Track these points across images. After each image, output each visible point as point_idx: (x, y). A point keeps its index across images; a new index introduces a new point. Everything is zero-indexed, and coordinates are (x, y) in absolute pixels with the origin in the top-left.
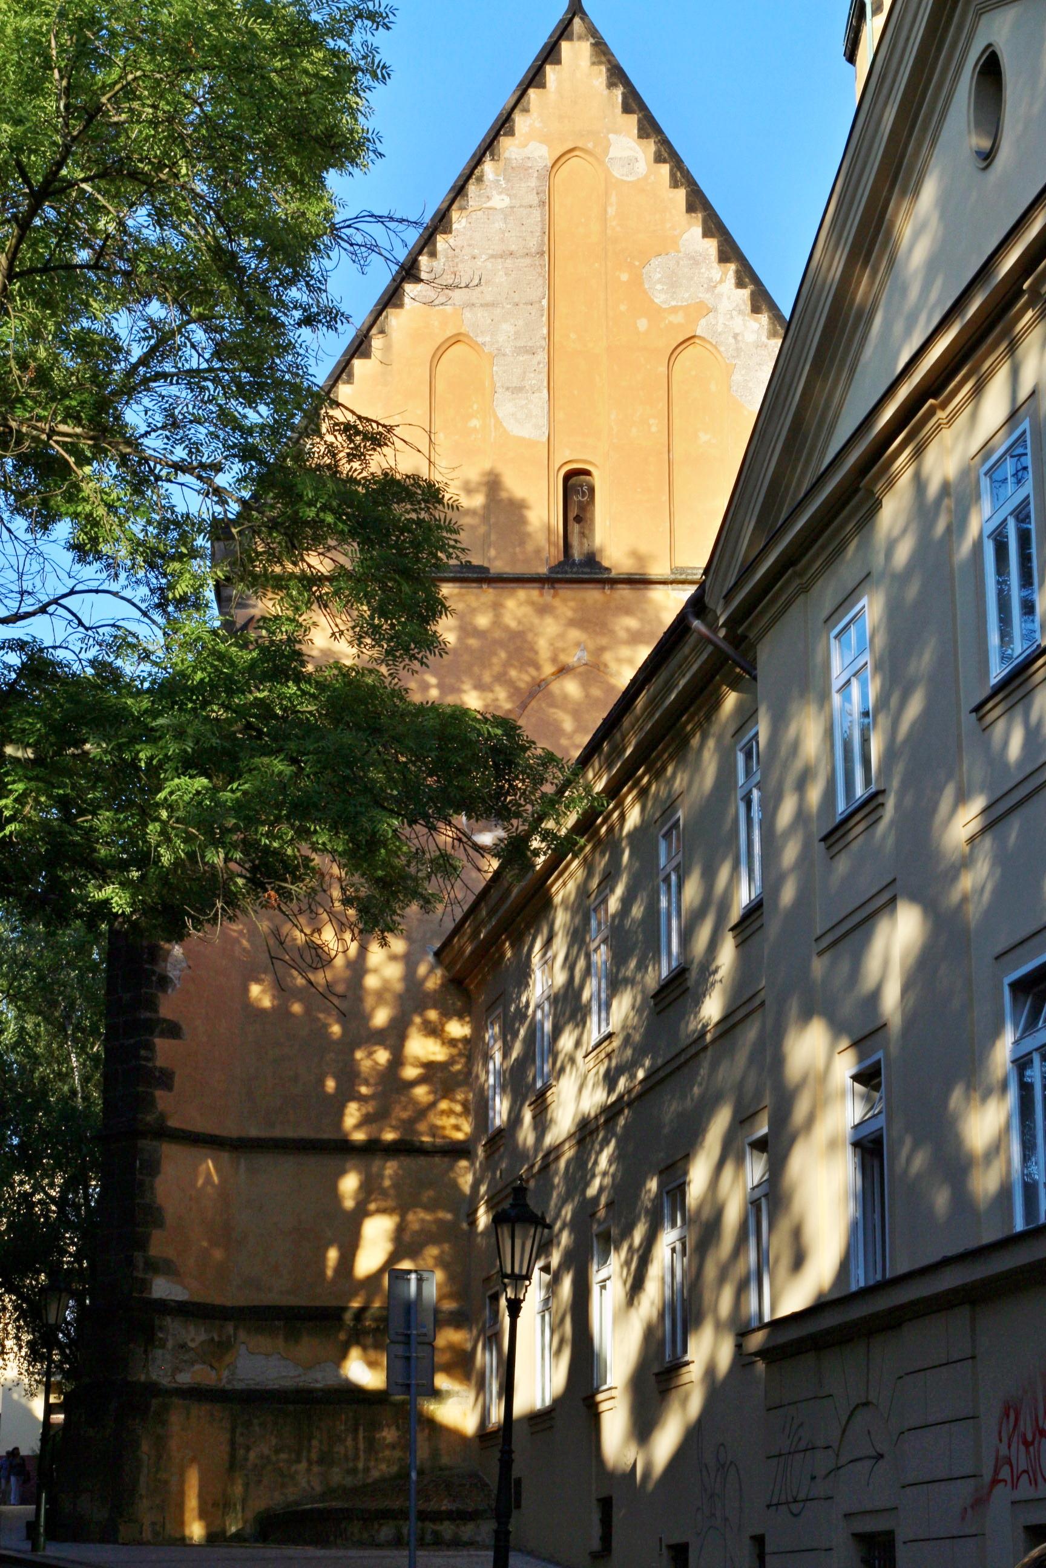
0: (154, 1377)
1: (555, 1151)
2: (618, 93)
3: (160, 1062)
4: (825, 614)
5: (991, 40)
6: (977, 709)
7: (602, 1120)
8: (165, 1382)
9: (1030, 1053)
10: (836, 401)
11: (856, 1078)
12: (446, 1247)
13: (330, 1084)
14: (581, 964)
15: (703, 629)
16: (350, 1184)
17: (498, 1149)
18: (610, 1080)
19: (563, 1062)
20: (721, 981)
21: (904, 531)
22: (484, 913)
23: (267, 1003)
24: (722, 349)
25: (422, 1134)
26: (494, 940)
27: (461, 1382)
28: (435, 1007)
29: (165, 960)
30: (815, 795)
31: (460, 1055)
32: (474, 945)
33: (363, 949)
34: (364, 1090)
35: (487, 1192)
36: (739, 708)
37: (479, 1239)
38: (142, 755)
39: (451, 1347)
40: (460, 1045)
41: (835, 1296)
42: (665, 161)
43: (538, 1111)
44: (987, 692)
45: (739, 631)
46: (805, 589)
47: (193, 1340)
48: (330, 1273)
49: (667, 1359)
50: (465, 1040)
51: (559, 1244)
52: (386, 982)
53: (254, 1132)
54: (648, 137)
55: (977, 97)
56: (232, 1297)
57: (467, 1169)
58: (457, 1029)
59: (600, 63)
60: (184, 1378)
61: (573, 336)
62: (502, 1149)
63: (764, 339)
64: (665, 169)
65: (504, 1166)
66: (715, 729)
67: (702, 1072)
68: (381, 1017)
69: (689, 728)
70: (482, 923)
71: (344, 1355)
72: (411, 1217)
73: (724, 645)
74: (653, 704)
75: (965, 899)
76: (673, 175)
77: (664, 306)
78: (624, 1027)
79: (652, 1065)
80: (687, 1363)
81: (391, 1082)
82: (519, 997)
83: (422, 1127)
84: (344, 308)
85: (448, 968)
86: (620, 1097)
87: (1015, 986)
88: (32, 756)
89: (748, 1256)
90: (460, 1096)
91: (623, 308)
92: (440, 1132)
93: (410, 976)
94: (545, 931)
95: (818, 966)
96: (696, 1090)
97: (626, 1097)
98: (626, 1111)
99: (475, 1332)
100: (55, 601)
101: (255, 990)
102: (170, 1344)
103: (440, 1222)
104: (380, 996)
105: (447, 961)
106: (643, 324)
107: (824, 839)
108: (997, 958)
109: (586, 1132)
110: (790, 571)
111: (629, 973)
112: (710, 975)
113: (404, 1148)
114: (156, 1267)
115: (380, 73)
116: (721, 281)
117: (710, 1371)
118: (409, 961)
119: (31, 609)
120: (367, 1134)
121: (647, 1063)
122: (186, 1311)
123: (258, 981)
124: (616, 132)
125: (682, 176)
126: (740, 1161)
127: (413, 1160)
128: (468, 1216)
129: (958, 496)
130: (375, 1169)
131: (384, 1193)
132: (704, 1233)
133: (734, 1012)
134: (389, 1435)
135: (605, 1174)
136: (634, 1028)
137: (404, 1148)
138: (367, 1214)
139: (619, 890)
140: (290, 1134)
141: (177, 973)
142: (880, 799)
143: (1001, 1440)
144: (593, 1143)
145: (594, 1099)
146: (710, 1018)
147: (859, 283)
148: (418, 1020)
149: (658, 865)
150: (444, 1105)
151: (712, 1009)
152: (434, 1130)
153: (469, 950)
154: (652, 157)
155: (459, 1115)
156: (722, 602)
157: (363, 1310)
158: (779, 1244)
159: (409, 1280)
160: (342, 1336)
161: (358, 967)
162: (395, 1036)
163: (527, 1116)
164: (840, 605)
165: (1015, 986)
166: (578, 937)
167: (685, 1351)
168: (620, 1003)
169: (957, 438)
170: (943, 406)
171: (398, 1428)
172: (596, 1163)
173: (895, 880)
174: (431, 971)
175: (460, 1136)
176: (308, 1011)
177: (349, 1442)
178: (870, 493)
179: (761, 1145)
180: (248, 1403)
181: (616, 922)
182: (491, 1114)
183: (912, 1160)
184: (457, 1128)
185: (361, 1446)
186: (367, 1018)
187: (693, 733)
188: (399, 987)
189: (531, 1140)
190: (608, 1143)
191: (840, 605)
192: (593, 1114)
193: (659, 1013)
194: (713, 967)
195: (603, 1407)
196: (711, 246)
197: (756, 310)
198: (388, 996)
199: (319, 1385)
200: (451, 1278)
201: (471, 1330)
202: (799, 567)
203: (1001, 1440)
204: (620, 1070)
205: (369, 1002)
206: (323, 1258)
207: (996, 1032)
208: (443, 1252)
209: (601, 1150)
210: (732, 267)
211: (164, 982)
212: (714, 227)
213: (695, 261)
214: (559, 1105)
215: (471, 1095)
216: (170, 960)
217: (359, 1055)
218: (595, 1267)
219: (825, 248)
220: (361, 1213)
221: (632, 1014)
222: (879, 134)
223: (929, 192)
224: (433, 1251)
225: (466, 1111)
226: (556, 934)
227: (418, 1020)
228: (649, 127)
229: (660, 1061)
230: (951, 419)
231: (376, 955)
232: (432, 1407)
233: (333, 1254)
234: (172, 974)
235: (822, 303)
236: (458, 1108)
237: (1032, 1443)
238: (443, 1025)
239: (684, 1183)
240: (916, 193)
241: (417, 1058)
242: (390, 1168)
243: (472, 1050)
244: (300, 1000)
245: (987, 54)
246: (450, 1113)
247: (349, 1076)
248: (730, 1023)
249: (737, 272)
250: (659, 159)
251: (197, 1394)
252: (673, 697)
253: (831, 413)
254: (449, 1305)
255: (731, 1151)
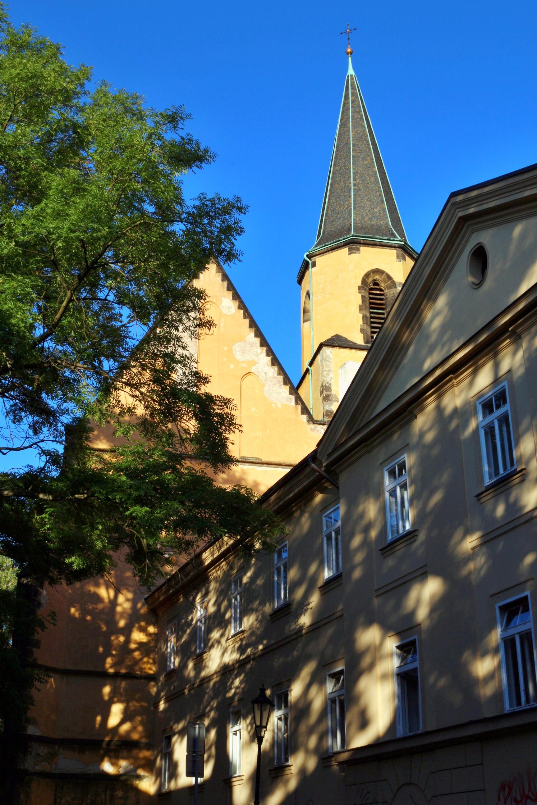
0: (26, 767)
1: (208, 678)
2: (226, 283)
3: (36, 637)
4: (381, 460)
5: (481, 240)
6: (477, 496)
7: (237, 665)
8: (30, 769)
9: (514, 634)
10: (387, 380)
11: (398, 647)
12: (144, 717)
13: (101, 649)
14: (225, 603)
15: (316, 467)
16: (107, 690)
17: (173, 677)
18: (241, 650)
19: (213, 643)
20: (311, 608)
21: (430, 429)
22: (174, 583)
23: (77, 615)
24: (261, 377)
25: (136, 671)
26: (176, 594)
27: (148, 772)
28: (143, 621)
29: (40, 596)
30: (373, 534)
31: (153, 640)
32: (165, 596)
33: (116, 597)
34: (114, 652)
35: (165, 695)
36: (323, 501)
37: (160, 714)
38: (117, 497)
39: (145, 758)
40: (153, 636)
41: (388, 739)
42: (241, 309)
43: (197, 662)
44: (484, 489)
45: (332, 469)
46: (369, 452)
47: (42, 752)
48: (97, 726)
49: (275, 764)
50: (154, 634)
51: (209, 716)
52: (124, 609)
53: (70, 667)
54: (236, 300)
55: (471, 262)
56: (57, 735)
57: (154, 686)
58: (151, 629)
59: (219, 272)
60: (38, 768)
61: (206, 368)
62: (175, 678)
63: (276, 375)
64: (242, 312)
65: (176, 684)
66: (309, 509)
67: (299, 645)
68: (122, 623)
69: (294, 509)
70: (172, 587)
71: (102, 760)
72: (131, 704)
73: (324, 474)
74: (279, 499)
75: (470, 573)
76: (244, 314)
77: (240, 360)
78: (250, 629)
79: (267, 643)
80: (289, 766)
81: (125, 649)
82: (187, 617)
83: (137, 668)
84: (215, 322)
85: (149, 605)
86: (248, 657)
87: (502, 608)
88: (51, 498)
89: (327, 721)
90: (152, 656)
91: (225, 360)
92: (144, 670)
93: (134, 607)
94: (204, 591)
95: (376, 602)
96: (295, 653)
97: (252, 656)
98: (252, 662)
99: (156, 752)
100: (36, 443)
101: (73, 610)
102: (33, 753)
103: (142, 706)
104: (122, 615)
105: (150, 602)
106: (232, 366)
107: (381, 550)
108: (491, 596)
109: (226, 671)
110: (364, 444)
111: (255, 606)
112: (304, 606)
113: (130, 676)
114: (29, 721)
115: (241, 231)
116: (261, 353)
117: (302, 771)
118: (134, 602)
119: (26, 446)
120: (115, 670)
121: (265, 642)
122: (42, 740)
123: (74, 607)
124: (224, 297)
125: (247, 314)
126: (322, 683)
127: (131, 683)
128: (154, 704)
129: (463, 414)
130: (117, 684)
131: (121, 694)
132: (301, 711)
133: (319, 622)
134: (119, 793)
135: (237, 688)
136: (257, 628)
137: (130, 676)
138: (114, 703)
139: (249, 574)
140: (85, 669)
141: (44, 601)
142: (416, 533)
143: (499, 800)
144: (231, 675)
145: (231, 657)
146: (304, 624)
147: (405, 333)
148: (137, 625)
149: (273, 563)
150: (145, 660)
151: (305, 620)
152: (141, 669)
153: (161, 599)
154: (237, 307)
155: (151, 664)
156: (326, 457)
157: (110, 741)
158: (351, 716)
159: (195, 728)
160: (102, 752)
161: (114, 603)
162: (127, 631)
163: (191, 665)
164: (385, 461)
165: (502, 608)
166: (223, 593)
167: (287, 760)
168: (248, 620)
169: (461, 392)
170: (456, 378)
171: (123, 791)
172: (232, 683)
173: (426, 565)
174: (143, 605)
175: (152, 672)
176: (93, 619)
177: (103, 796)
178: (411, 412)
179: (336, 676)
180: (62, 779)
181: (247, 586)
182: (168, 663)
183: (435, 681)
184: (150, 669)
185: (108, 798)
186: (116, 623)
187: (296, 511)
188: (129, 611)
189: (192, 674)
190: (240, 676)
191: (385, 461)
192: (231, 663)
193: (272, 623)
194: (306, 603)
195: (234, 784)
196: (257, 341)
197: (273, 365)
198: (125, 615)
199: (91, 772)
200: (146, 729)
201: (153, 751)
202: (368, 442)
203: (499, 800)
204: (248, 646)
205: (118, 617)
206: (95, 720)
207: (491, 627)
208: (143, 719)
209: (236, 678)
210: (265, 349)
211: (39, 604)
212: (259, 334)
213: (252, 345)
214: (209, 660)
215: (157, 656)
216: (42, 596)
217: (113, 638)
218: (231, 726)
219: (392, 319)
220: (111, 702)
221: (256, 623)
222: (421, 279)
223: (442, 301)
224: (139, 718)
225: (154, 663)
226: (211, 592)
227: (137, 625)
228: (236, 296)
229: (273, 642)
230: (458, 384)
231: (121, 599)
232: (137, 782)
233: (99, 718)
234: (43, 601)
235: (387, 342)
236: (151, 661)
237: (521, 801)
238: (147, 628)
239: (288, 691)
240: (435, 300)
241: (135, 641)
242: (123, 684)
243: (159, 639)
244: (89, 615)
245: (477, 246)
246: (148, 663)
247: (108, 647)
248: (315, 627)
249: (267, 351)
250: (239, 308)
251: (43, 775)
252: (291, 496)
253: (385, 383)
254: (144, 740)
255: (317, 679)
